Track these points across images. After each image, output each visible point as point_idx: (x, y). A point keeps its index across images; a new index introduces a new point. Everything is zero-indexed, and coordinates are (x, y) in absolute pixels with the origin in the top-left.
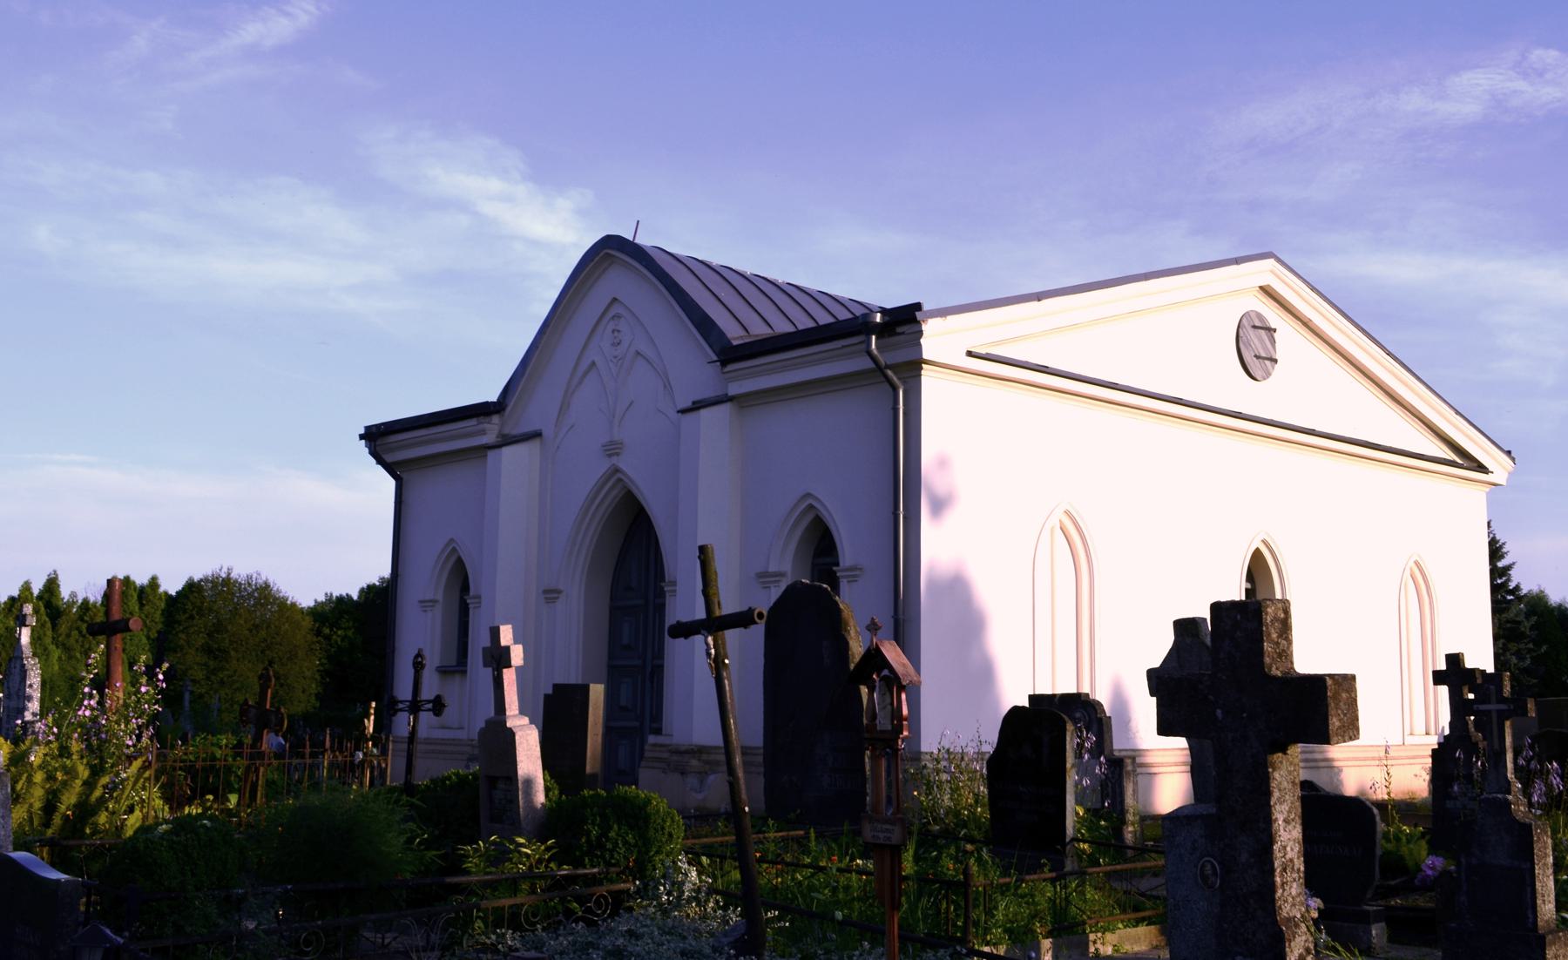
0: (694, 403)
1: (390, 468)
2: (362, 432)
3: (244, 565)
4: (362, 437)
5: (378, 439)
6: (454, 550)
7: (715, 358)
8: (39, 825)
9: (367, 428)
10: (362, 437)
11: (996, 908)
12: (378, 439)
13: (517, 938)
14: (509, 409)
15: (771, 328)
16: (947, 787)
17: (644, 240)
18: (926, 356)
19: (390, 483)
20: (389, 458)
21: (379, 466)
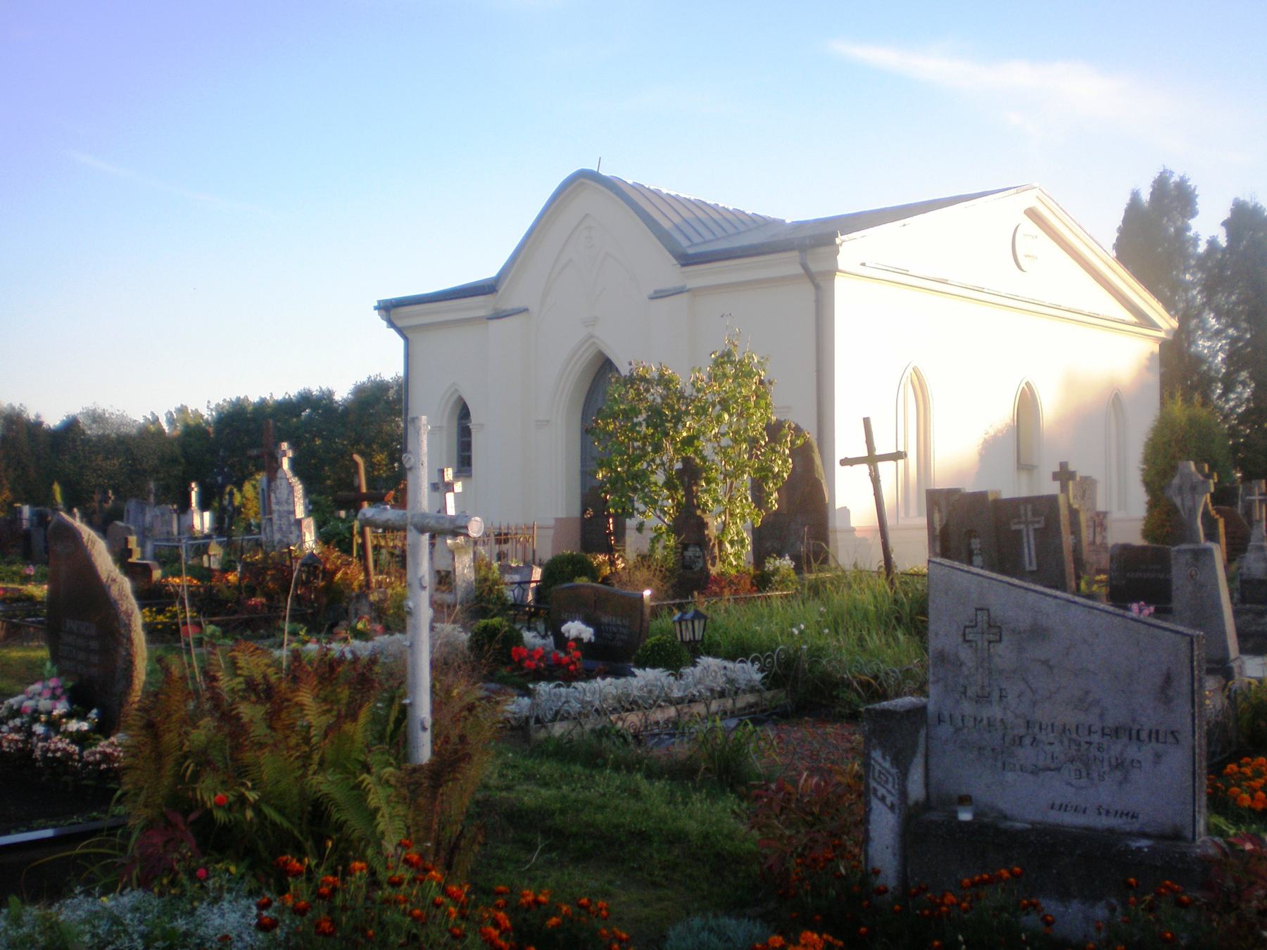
0: (656, 292)
1: (400, 331)
2: (376, 304)
3: (315, 386)
4: (376, 308)
5: (390, 309)
6: (456, 390)
7: (676, 263)
8: (810, 581)
9: (379, 302)
10: (376, 308)
11: (667, 721)
12: (390, 309)
13: (307, 638)
14: (500, 292)
15: (1010, 188)
16: (913, 656)
17: (605, 172)
18: (840, 267)
19: (400, 342)
20: (399, 324)
21: (1117, 235)
